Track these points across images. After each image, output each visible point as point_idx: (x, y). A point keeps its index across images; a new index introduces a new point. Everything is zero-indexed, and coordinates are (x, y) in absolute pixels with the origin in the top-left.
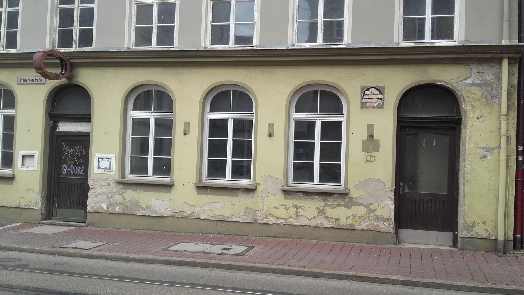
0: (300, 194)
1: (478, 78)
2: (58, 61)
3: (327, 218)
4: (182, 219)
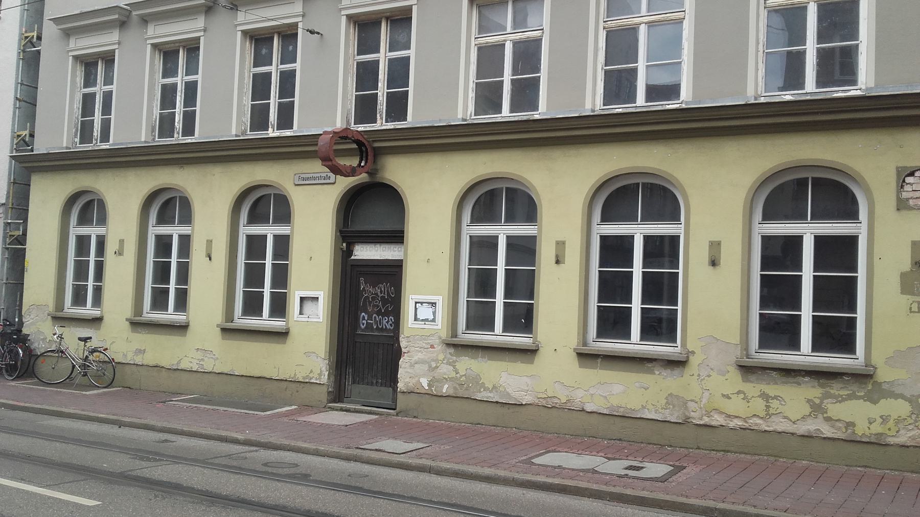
2: (355, 146)
4: (554, 409)
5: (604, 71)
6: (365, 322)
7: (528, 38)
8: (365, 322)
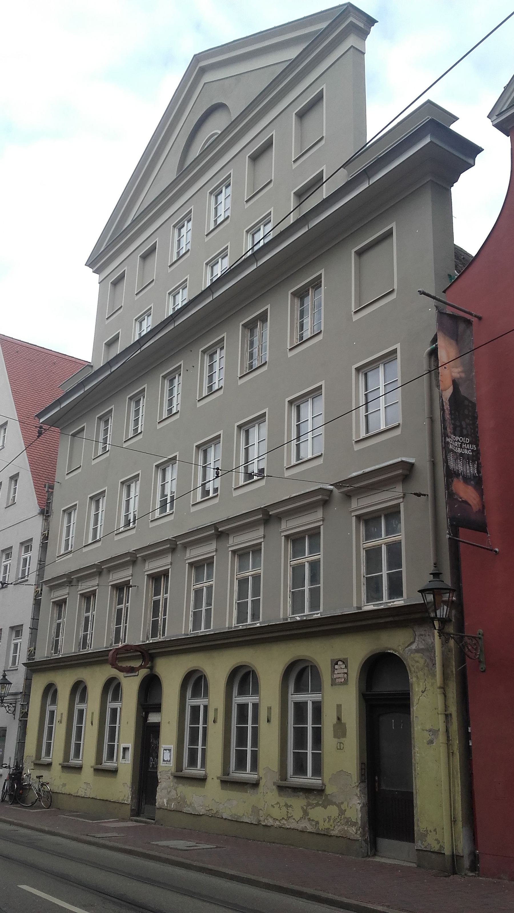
0: (290, 790)
1: (421, 642)
2: (139, 653)
3: (309, 820)
4: (212, 818)
5: (365, 578)
6: (151, 763)
7: (373, 546)
8: (151, 763)
